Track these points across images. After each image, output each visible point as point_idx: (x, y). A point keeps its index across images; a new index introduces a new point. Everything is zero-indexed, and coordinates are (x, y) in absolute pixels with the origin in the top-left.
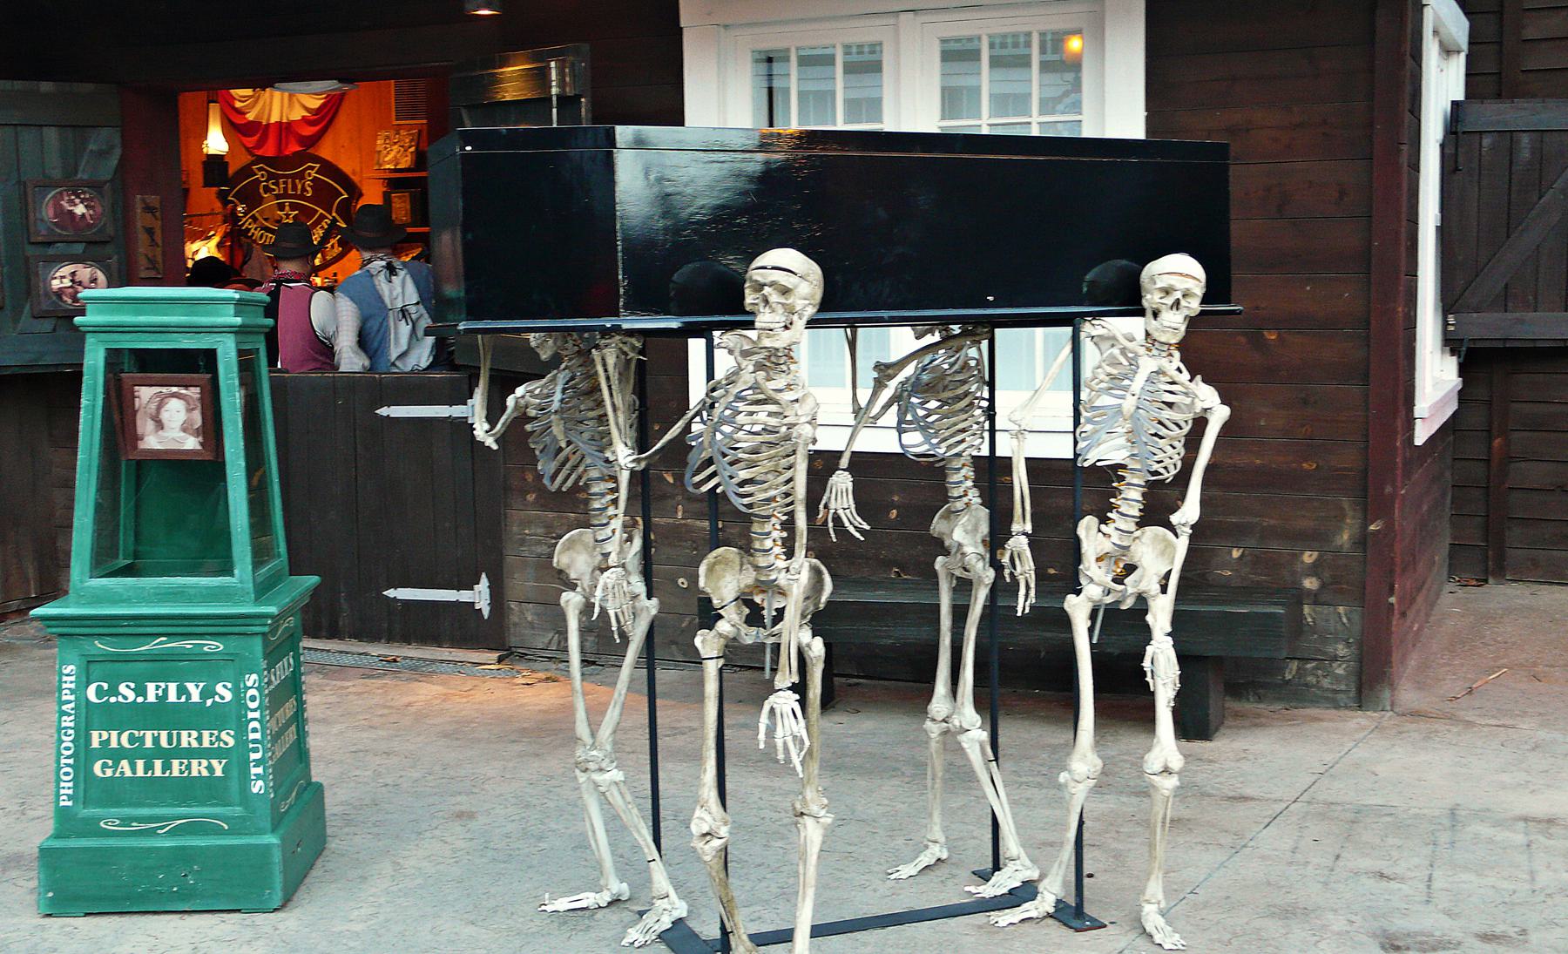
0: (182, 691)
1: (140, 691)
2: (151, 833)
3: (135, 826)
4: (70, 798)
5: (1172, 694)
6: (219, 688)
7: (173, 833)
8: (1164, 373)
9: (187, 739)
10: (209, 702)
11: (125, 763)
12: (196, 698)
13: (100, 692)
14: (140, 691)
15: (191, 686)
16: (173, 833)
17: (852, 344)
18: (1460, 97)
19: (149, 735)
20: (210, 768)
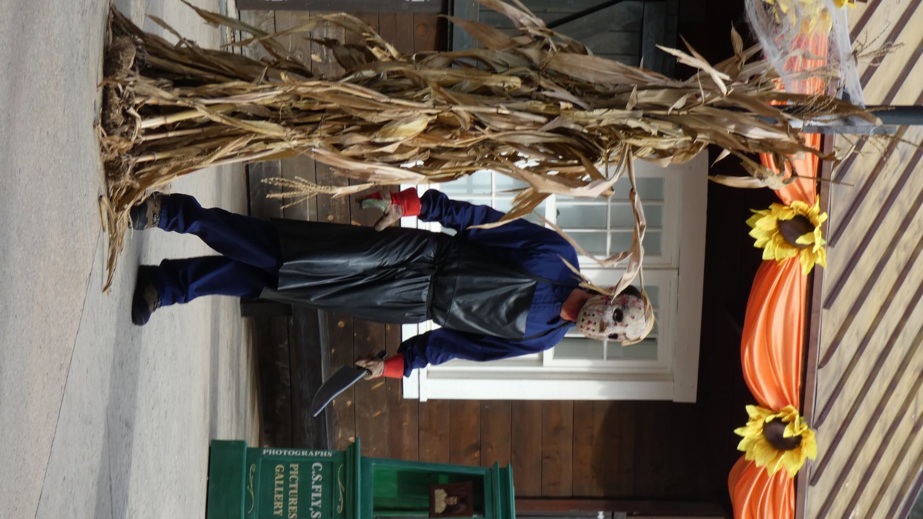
0: (317, 499)
1: (317, 483)
2: (248, 483)
3: (251, 478)
4: (292, 469)
5: (669, 80)
6: (317, 513)
7: (248, 493)
8: (558, 47)
9: (293, 501)
10: (311, 509)
11: (282, 476)
12: (313, 504)
13: (317, 468)
14: (317, 483)
15: (320, 502)
16: (248, 493)
17: (904, 141)
18: (625, 514)
19: (296, 485)
20: (278, 509)
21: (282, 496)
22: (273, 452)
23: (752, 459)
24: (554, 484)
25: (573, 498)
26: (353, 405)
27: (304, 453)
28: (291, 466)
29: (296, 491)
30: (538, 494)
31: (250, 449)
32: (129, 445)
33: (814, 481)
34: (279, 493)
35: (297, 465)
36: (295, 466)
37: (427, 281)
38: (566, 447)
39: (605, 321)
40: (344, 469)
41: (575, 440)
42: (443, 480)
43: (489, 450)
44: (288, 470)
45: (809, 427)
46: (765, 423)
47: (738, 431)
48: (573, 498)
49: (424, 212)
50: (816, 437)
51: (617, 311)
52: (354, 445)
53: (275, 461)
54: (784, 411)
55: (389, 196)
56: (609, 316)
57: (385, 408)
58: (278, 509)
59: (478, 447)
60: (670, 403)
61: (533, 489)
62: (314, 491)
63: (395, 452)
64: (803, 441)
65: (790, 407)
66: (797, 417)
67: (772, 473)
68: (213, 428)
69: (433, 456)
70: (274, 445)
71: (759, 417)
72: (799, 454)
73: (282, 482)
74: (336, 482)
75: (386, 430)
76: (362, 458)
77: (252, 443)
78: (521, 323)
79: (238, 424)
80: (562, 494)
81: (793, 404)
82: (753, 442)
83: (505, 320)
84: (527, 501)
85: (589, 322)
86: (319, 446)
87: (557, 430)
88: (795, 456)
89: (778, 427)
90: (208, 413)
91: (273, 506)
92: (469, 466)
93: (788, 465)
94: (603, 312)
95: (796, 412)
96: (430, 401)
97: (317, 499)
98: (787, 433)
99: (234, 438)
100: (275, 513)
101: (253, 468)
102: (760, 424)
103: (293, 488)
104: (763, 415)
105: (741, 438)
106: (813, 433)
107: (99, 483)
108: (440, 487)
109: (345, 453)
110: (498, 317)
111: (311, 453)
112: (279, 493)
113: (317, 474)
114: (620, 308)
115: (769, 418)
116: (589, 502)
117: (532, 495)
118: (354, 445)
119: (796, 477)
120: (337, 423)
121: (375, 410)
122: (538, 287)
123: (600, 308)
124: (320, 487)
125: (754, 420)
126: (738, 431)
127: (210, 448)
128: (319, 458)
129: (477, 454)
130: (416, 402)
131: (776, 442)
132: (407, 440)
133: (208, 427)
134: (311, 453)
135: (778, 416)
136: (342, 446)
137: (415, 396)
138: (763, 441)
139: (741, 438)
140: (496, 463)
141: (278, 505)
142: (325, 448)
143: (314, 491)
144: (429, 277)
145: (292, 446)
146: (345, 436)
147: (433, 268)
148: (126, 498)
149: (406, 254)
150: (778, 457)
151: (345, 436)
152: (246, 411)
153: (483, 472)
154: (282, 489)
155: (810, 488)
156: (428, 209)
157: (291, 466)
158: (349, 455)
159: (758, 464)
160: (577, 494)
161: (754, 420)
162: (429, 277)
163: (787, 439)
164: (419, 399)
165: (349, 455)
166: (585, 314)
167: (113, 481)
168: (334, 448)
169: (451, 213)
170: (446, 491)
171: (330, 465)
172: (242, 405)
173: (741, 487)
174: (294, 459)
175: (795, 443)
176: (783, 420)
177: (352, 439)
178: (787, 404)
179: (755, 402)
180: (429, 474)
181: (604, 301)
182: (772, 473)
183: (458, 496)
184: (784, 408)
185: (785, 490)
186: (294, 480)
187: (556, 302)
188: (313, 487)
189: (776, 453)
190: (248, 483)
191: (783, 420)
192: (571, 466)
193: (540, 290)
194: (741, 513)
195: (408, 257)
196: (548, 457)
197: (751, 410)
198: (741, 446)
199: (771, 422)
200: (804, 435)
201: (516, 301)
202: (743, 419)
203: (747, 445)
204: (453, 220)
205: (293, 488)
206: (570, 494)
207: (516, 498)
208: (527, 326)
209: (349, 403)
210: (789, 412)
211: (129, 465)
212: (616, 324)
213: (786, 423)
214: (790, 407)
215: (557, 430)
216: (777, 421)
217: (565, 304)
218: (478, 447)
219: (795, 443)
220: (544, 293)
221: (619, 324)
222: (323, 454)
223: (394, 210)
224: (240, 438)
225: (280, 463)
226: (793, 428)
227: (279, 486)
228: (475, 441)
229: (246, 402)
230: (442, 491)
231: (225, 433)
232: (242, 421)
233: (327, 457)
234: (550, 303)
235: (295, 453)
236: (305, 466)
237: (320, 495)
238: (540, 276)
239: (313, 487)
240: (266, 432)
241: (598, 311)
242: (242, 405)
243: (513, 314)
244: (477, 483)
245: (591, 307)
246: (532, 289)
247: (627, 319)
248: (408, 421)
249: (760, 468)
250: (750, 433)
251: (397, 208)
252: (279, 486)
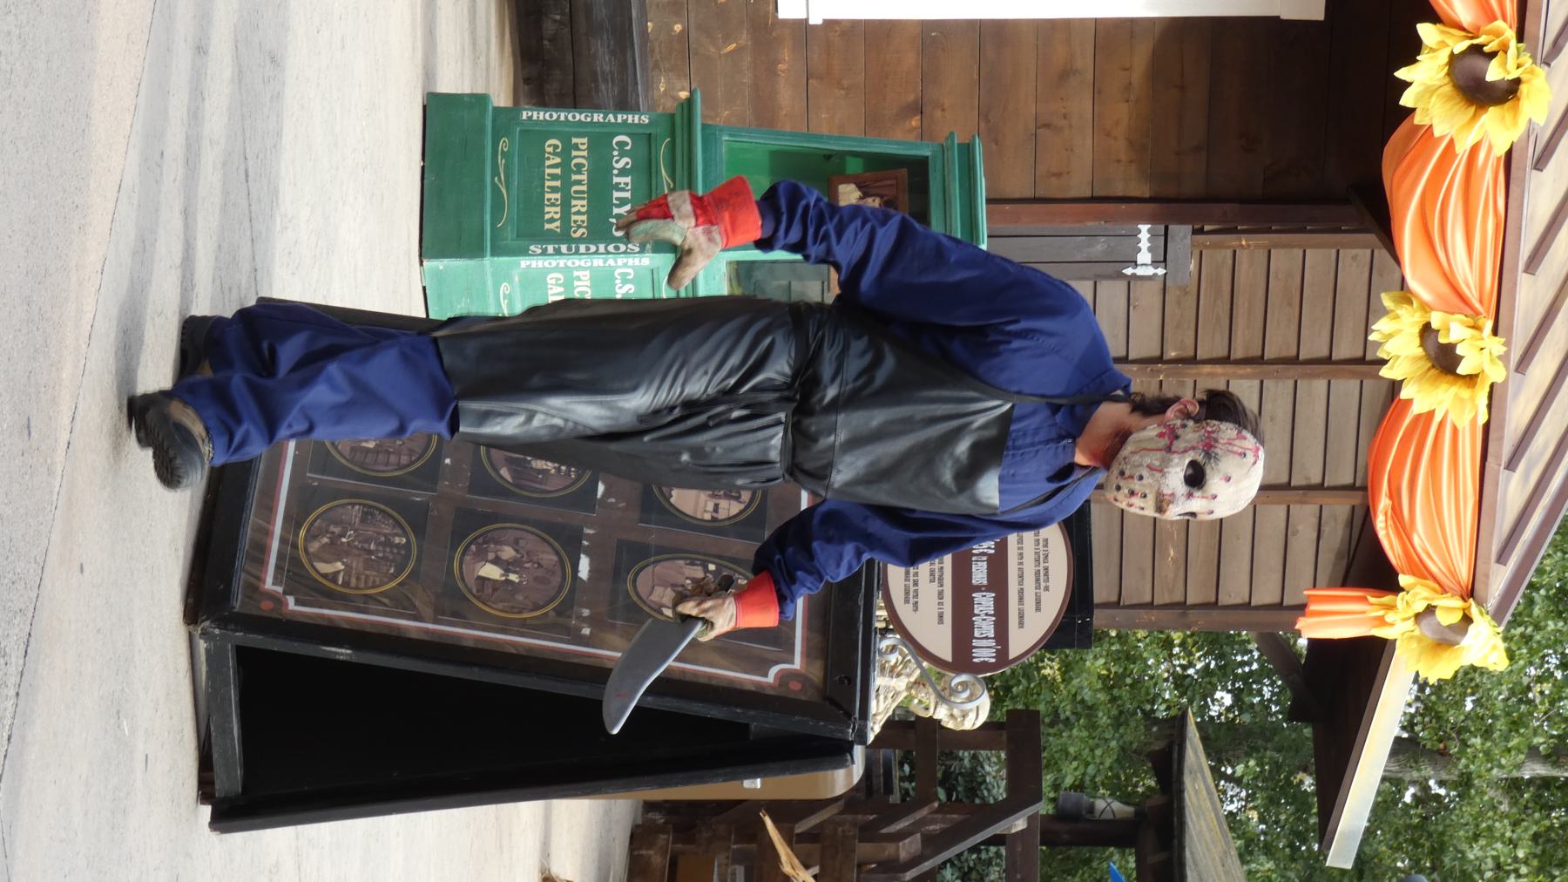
0: (623, 202)
1: (623, 172)
2: (495, 172)
3: (501, 162)
9: (580, 205)
11: (558, 160)
12: (616, 211)
13: (621, 144)
19: (584, 177)
20: (552, 220)
21: (558, 196)
22: (540, 115)
23: (1426, 122)
24: (1058, 175)
25: (1093, 199)
26: (686, 33)
27: (598, 117)
28: (574, 140)
29: (584, 188)
30: (1029, 194)
31: (496, 109)
32: (278, 96)
33: (1540, 163)
34: (554, 190)
35: (585, 140)
36: (582, 142)
37: (778, 423)
38: (1081, 105)
39: (1167, 491)
40: (673, 144)
41: (1096, 91)
42: (854, 166)
43: (938, 113)
44: (568, 148)
45: (1535, 62)
46: (1452, 55)
47: (1402, 74)
48: (1093, 199)
49: (768, 234)
50: (1548, 78)
51: (1193, 464)
52: (690, 102)
53: (546, 131)
54: (1488, 33)
55: (687, 208)
56: (1175, 478)
57: (744, 38)
58: (552, 220)
59: (918, 108)
60: (1276, 20)
61: (1019, 185)
62: (617, 187)
63: (765, 115)
64: (1523, 88)
65: (1499, 24)
66: (1513, 43)
67: (1462, 148)
68: (429, 73)
69: (836, 125)
70: (542, 102)
71: (1443, 44)
72: (1516, 110)
73: (558, 171)
74: (658, 172)
75: (747, 79)
76: (704, 126)
77: (501, 97)
78: (989, 489)
79: (478, 65)
80: (1073, 194)
81: (1505, 19)
82: (1430, 91)
83: (953, 488)
84: (1008, 207)
85: (1132, 493)
86: (624, 105)
87: (1066, 74)
88: (1508, 117)
89: (1477, 62)
90: (419, 44)
91: (544, 213)
92: (900, 142)
93: (1496, 130)
94: (1160, 471)
95: (1510, 34)
96: (829, 24)
97: (623, 202)
98: (1494, 73)
99: (468, 91)
100: (547, 226)
101: (504, 145)
102: (1443, 56)
103: (579, 182)
104: (1449, 41)
105: (1406, 85)
106: (1541, 71)
107: (224, 164)
108: (847, 180)
109: (673, 116)
110: (936, 482)
111: (611, 116)
112: (554, 190)
113: (621, 156)
114: (1200, 458)
115: (1461, 46)
116: (1123, 206)
117: (1017, 195)
118: (690, 102)
119: (1509, 154)
120: (656, 66)
121: (727, 39)
122: (1016, 413)
123: (1154, 459)
124: (628, 180)
125: (1432, 50)
126: (1402, 74)
127: (424, 108)
128: (625, 128)
129: (915, 122)
130: (802, 26)
131: (1477, 90)
132: (787, 96)
133: (419, 70)
134: (611, 116)
135: (1475, 42)
136: (670, 106)
137: (799, 14)
138: (1448, 89)
139: (1406, 85)
140: (952, 134)
141: (552, 212)
142: (634, 109)
143: (617, 187)
144: (782, 416)
145: (575, 105)
146: (670, 89)
147: (789, 400)
148: (274, 193)
149: (729, 376)
150: (1475, 117)
151: (670, 89)
152: (488, 42)
153: (928, 153)
154: (558, 183)
155: (1535, 172)
156: (776, 230)
157: (574, 140)
158: (681, 121)
159: (1437, 133)
160: (1099, 193)
161: (1432, 50)
162: (782, 416)
163: (1492, 84)
164: (807, 20)
165: (681, 121)
166: (1122, 473)
167: (250, 163)
168: (651, 109)
169: (826, 237)
170: (860, 187)
171: (645, 139)
172: (481, 32)
173: (1406, 173)
174: (581, 129)
175: (1508, 92)
176: (1486, 49)
177: (684, 95)
178: (1493, 18)
179: (1434, 17)
180: (828, 156)
181: (1164, 442)
182: (1462, 148)
183: (882, 197)
184: (1489, 27)
185: (1489, 177)
186: (579, 166)
187: (1061, 438)
188: (616, 180)
189: (1472, 109)
190: (495, 172)
191: (1486, 49)
192: (1089, 141)
193: (1022, 418)
194: (1407, 208)
195: (732, 381)
196: (1047, 126)
197: (1426, 30)
198: (1407, 100)
199: (1463, 54)
200: (1524, 77)
201: (975, 447)
202: (1411, 50)
203: (1419, 97)
204: (829, 251)
205: (579, 182)
206: (1088, 194)
207: (989, 201)
208: (1001, 492)
209: (678, 28)
210: (1498, 34)
211: (279, 134)
212: (1190, 495)
213: (1493, 55)
214: (1499, 24)
215: (1066, 74)
216: (1476, 50)
217: (1080, 440)
218: (918, 108)
219: (1508, 92)
220: (1036, 422)
221: (1197, 494)
222: (632, 118)
223: (702, 239)
224: (480, 90)
225: (554, 135)
226: (1504, 64)
227: (554, 177)
228: (911, 98)
229: (488, 22)
230: (852, 187)
231: (448, 84)
232: (483, 59)
233: (639, 125)
234: (1047, 442)
235: (580, 117)
236: (600, 141)
237: (628, 195)
238: (1019, 393)
239: (616, 180)
240: (527, 81)
241: (1150, 468)
242: (481, 32)
243: (969, 473)
244: (918, 169)
245: (1137, 457)
246: (1006, 419)
247: (1214, 483)
248: (787, 61)
249: (1441, 138)
250: (1424, 81)
251: (708, 233)
252: (554, 177)
